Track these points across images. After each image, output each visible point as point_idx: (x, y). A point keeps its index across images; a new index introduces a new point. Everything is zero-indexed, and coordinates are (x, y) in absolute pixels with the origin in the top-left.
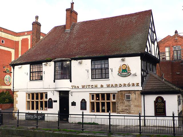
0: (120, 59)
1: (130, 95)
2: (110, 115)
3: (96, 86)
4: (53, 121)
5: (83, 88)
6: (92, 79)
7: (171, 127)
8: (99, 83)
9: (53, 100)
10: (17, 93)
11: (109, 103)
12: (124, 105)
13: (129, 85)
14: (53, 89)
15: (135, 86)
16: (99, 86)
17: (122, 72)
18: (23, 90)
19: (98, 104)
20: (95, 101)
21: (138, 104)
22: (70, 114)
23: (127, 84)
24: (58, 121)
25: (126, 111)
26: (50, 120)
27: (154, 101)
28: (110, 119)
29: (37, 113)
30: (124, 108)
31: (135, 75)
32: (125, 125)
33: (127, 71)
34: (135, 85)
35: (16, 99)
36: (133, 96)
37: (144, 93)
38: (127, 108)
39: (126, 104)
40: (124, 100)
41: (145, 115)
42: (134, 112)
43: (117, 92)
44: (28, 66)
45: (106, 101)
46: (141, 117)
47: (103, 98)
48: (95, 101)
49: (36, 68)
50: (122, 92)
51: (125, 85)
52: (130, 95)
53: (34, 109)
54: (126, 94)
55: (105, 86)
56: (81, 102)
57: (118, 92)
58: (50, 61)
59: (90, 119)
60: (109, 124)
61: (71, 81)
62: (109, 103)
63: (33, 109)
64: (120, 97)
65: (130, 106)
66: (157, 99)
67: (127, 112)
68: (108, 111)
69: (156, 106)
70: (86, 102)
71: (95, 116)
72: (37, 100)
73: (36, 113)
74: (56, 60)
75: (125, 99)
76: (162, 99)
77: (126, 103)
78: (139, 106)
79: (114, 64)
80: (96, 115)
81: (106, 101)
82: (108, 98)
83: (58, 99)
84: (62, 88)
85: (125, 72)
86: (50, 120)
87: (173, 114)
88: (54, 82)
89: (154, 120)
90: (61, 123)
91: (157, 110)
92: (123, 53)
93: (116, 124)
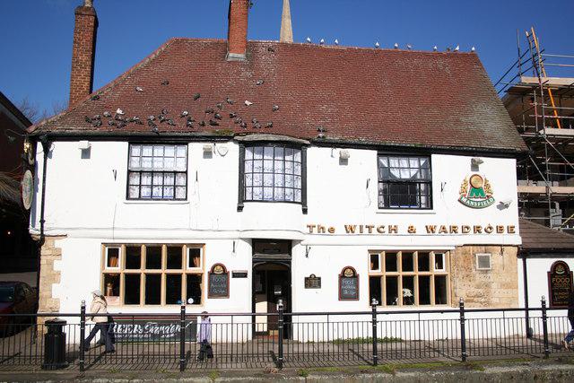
3: (393, 230)
4: (224, 341)
7: (540, 341)
8: (402, 217)
9: (230, 269)
10: (58, 243)
11: (428, 278)
12: (472, 283)
13: (489, 230)
14: (237, 235)
15: (437, 233)
16: (403, 230)
17: (471, 194)
19: (392, 282)
20: (120, 268)
21: (508, 280)
22: (293, 311)
23: (484, 226)
27: (548, 273)
29: (183, 312)
30: (474, 291)
31: (503, 206)
33: (482, 194)
34: (460, 231)
35: (50, 264)
36: (495, 259)
37: (524, 253)
40: (474, 271)
41: (524, 307)
43: (454, 248)
45: (416, 273)
46: (530, 312)
47: (408, 265)
48: (381, 271)
49: (405, 169)
51: (477, 230)
52: (488, 257)
53: (160, 304)
55: (421, 230)
56: (342, 276)
57: (457, 247)
59: (511, 323)
60: (459, 337)
61: (305, 211)
62: (428, 278)
64: (461, 263)
65: (487, 285)
66: (555, 267)
67: (481, 303)
69: (551, 285)
70: (355, 276)
71: (417, 314)
73: (180, 312)
74: (247, 138)
75: (475, 267)
76: (565, 266)
77: (479, 278)
78: (513, 286)
79: (449, 171)
80: (419, 312)
81: (416, 273)
82: (424, 265)
83: (247, 266)
85: (476, 194)
87: (83, 308)
88: (240, 209)
91: (556, 294)
92: (474, 144)
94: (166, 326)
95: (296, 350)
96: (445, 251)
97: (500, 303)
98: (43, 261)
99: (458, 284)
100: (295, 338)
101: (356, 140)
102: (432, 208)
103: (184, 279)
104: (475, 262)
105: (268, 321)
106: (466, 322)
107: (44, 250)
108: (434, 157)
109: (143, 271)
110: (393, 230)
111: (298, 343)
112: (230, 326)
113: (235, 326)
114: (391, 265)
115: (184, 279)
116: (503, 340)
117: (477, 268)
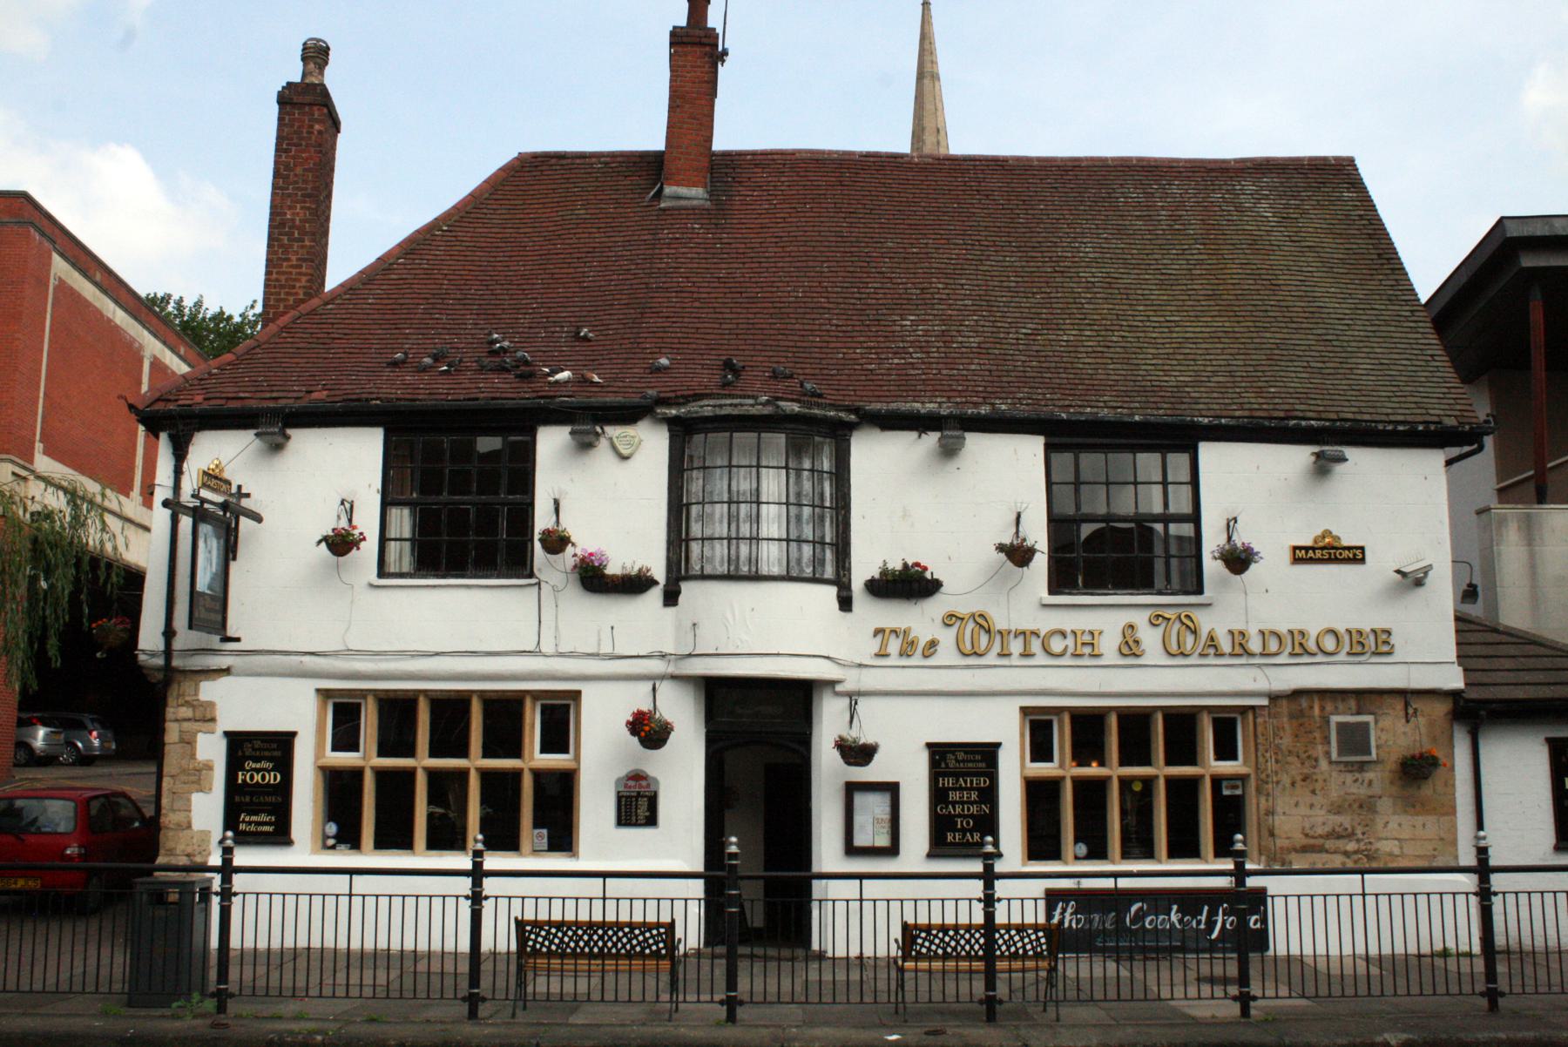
0: (1299, 457)
1: (1367, 724)
2: (477, 866)
5: (916, 660)
6: (382, 573)
11: (1193, 783)
12: (1318, 800)
14: (657, 666)
18: (307, 659)
20: (366, 757)
22: (816, 869)
24: (513, 947)
25: (1340, 844)
26: (54, 941)
28: (477, 898)
30: (1322, 821)
32: (1347, 950)
35: (189, 742)
38: (1345, 820)
39: (1335, 793)
40: (1324, 764)
42: (1397, 851)
43: (1265, 702)
44: (1031, 448)
48: (366, 757)
50: (1304, 703)
54: (1335, 719)
57: (1274, 697)
58: (628, 415)
60: (465, 945)
63: (1183, 845)
67: (1346, 854)
68: (1223, 849)
72: (1093, 770)
75: (1328, 754)
82: (504, 737)
84: (734, 660)
86: (54, 941)
89: (330, 901)
90: (758, 967)
93: (369, 946)
94: (1105, 912)
95: (827, 977)
96: (1243, 710)
97: (1402, 855)
98: (172, 733)
99: (1283, 803)
100: (815, 946)
101: (984, 410)
102: (1199, 590)
103: (527, 783)
104: (1326, 740)
105: (707, 891)
106: (237, 901)
107: (175, 711)
108: (1211, 454)
109: (423, 761)
110: (1086, 648)
111: (821, 956)
112: (855, 906)
113: (868, 906)
114: (396, 738)
115: (527, 783)
116: (1348, 963)
117: (1334, 756)
